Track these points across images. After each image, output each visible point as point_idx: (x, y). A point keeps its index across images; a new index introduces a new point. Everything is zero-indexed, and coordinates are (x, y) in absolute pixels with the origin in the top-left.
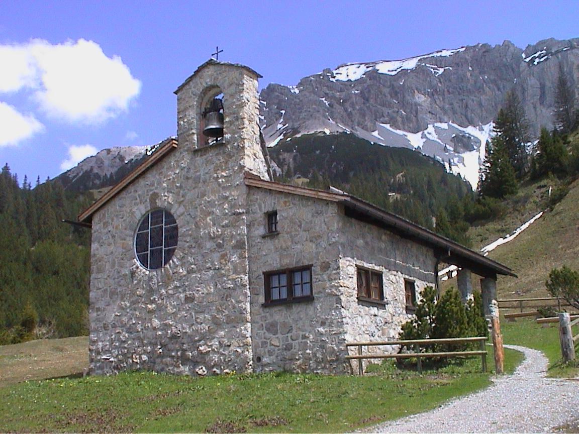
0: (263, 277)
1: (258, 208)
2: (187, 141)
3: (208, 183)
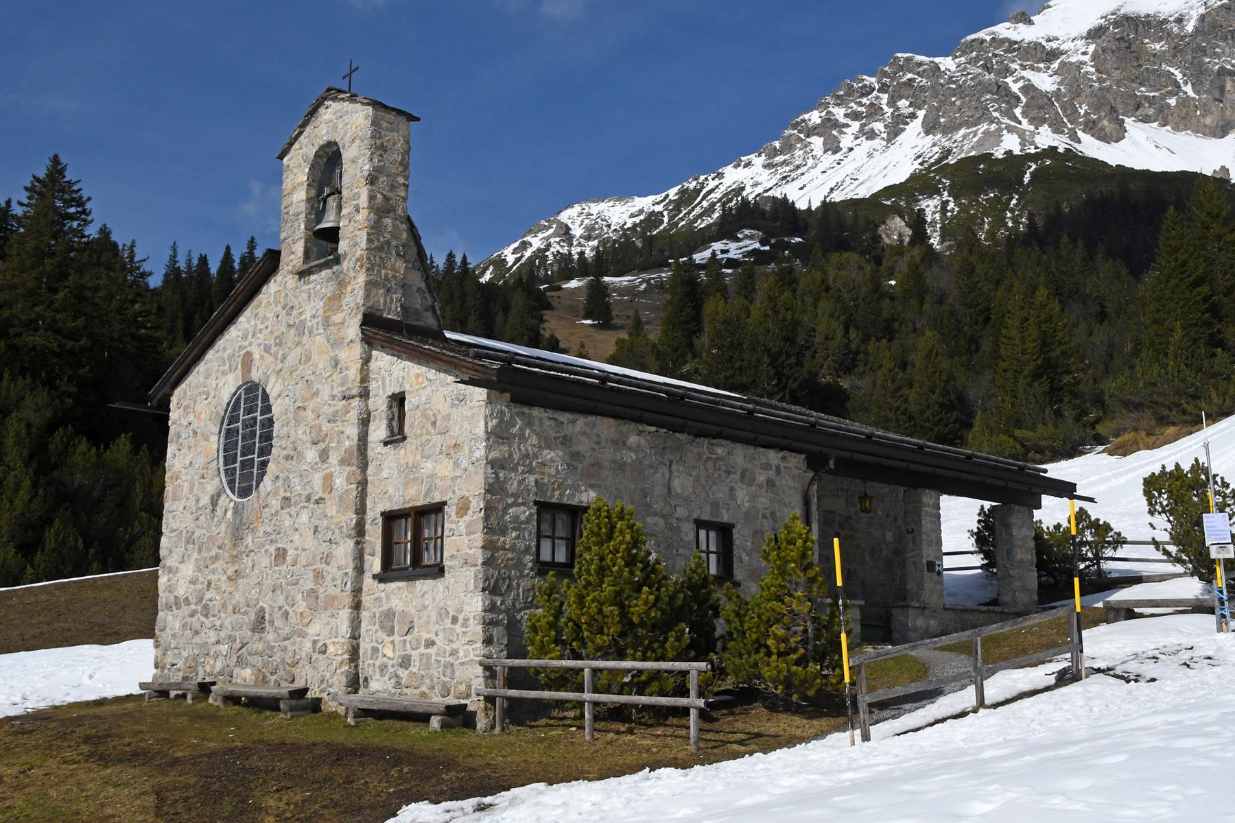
0: (380, 520)
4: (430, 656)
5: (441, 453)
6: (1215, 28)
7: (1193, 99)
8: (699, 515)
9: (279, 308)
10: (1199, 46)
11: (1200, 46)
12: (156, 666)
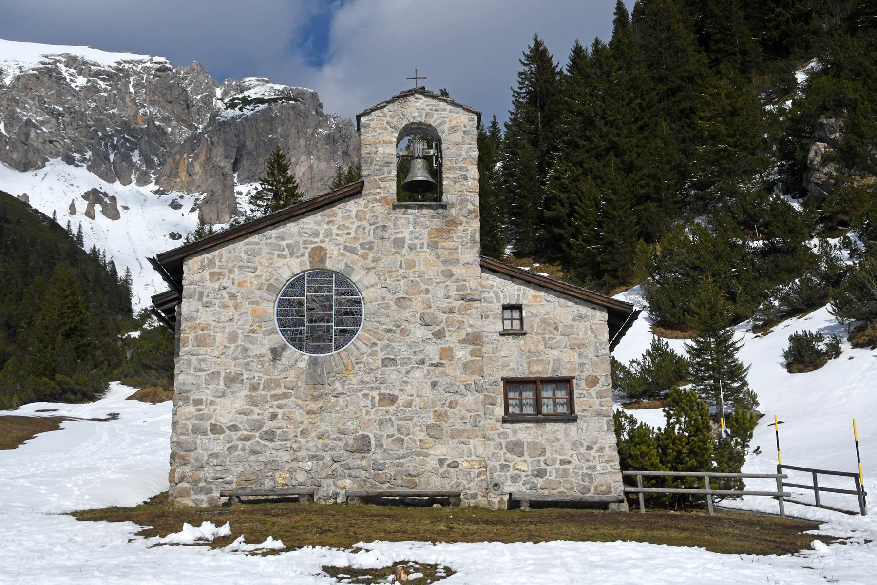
1: (494, 297)
2: (380, 188)
3: (419, 252)
4: (566, 471)
5: (566, 347)
6: (27, 89)
7: (5, 136)
10: (13, 99)
11: (14, 98)
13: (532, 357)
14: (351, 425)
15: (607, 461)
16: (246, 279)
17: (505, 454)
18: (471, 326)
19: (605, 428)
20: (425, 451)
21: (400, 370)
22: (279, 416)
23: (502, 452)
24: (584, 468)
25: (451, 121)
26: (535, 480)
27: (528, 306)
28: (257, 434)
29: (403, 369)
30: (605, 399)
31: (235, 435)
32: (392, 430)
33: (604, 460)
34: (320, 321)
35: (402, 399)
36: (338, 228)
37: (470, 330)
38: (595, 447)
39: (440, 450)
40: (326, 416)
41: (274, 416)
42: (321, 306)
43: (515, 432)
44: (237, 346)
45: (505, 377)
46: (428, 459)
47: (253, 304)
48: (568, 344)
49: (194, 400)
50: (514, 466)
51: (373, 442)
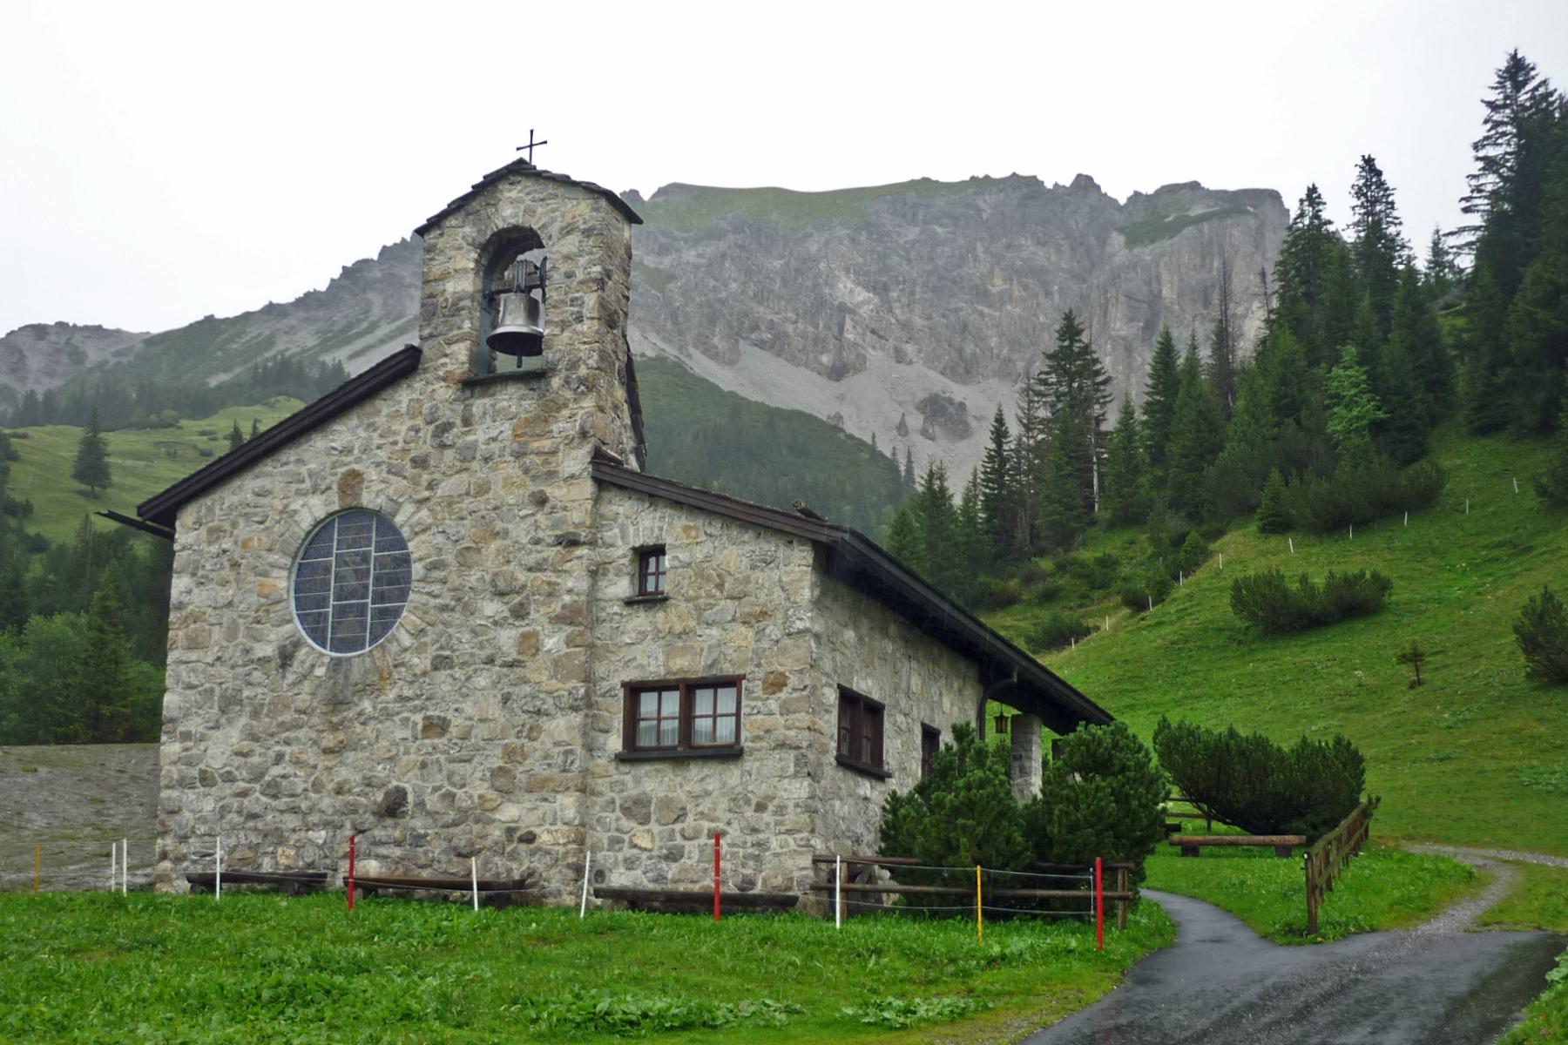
0: (621, 693)
8: (1556, 592)
9: (419, 422)
12: (1392, 203)
13: (677, 638)
14: (381, 771)
15: (788, 832)
16: (252, 535)
17: (617, 819)
18: (570, 591)
19: (792, 769)
20: (489, 814)
21: (457, 676)
22: (287, 758)
23: (613, 816)
24: (749, 844)
25: (563, 216)
26: (664, 865)
27: (675, 547)
28: (258, 787)
29: (458, 673)
30: (794, 716)
31: (228, 789)
32: (440, 779)
33: (783, 829)
34: (353, 598)
35: (457, 722)
36: (381, 436)
37: (567, 598)
38: (771, 808)
39: (509, 812)
40: (350, 756)
41: (279, 758)
42: (355, 571)
43: (638, 781)
44: (236, 646)
45: (627, 680)
46: (490, 829)
47: (260, 575)
48: (738, 615)
49: (181, 733)
50: (631, 842)
51: (411, 798)
